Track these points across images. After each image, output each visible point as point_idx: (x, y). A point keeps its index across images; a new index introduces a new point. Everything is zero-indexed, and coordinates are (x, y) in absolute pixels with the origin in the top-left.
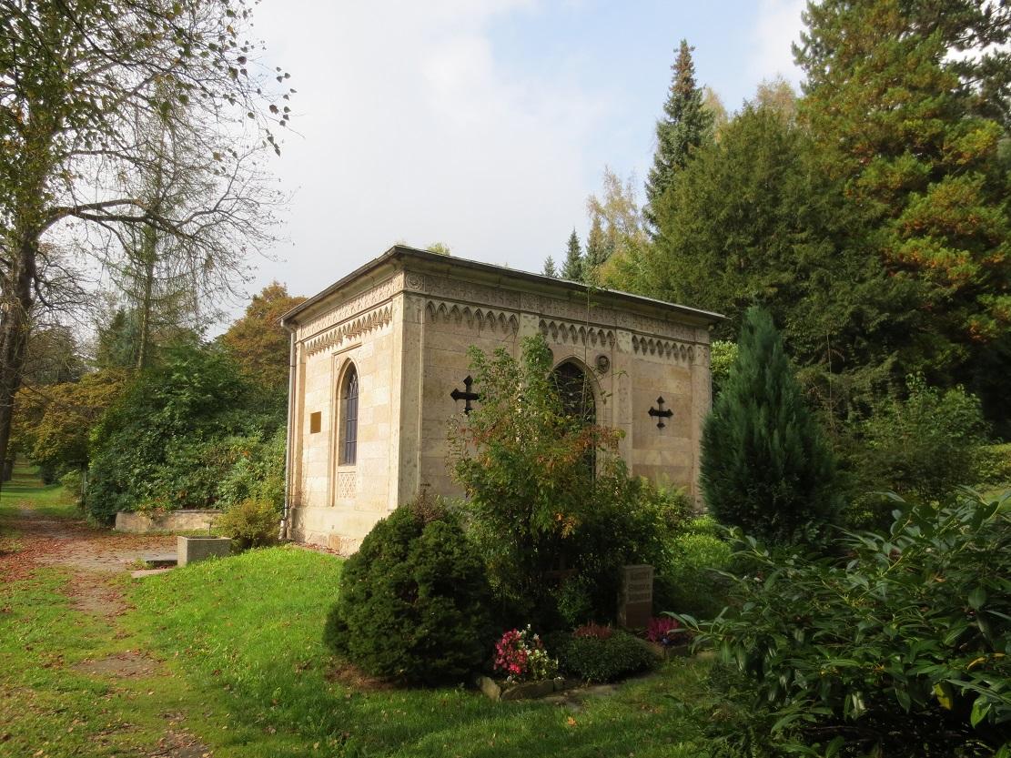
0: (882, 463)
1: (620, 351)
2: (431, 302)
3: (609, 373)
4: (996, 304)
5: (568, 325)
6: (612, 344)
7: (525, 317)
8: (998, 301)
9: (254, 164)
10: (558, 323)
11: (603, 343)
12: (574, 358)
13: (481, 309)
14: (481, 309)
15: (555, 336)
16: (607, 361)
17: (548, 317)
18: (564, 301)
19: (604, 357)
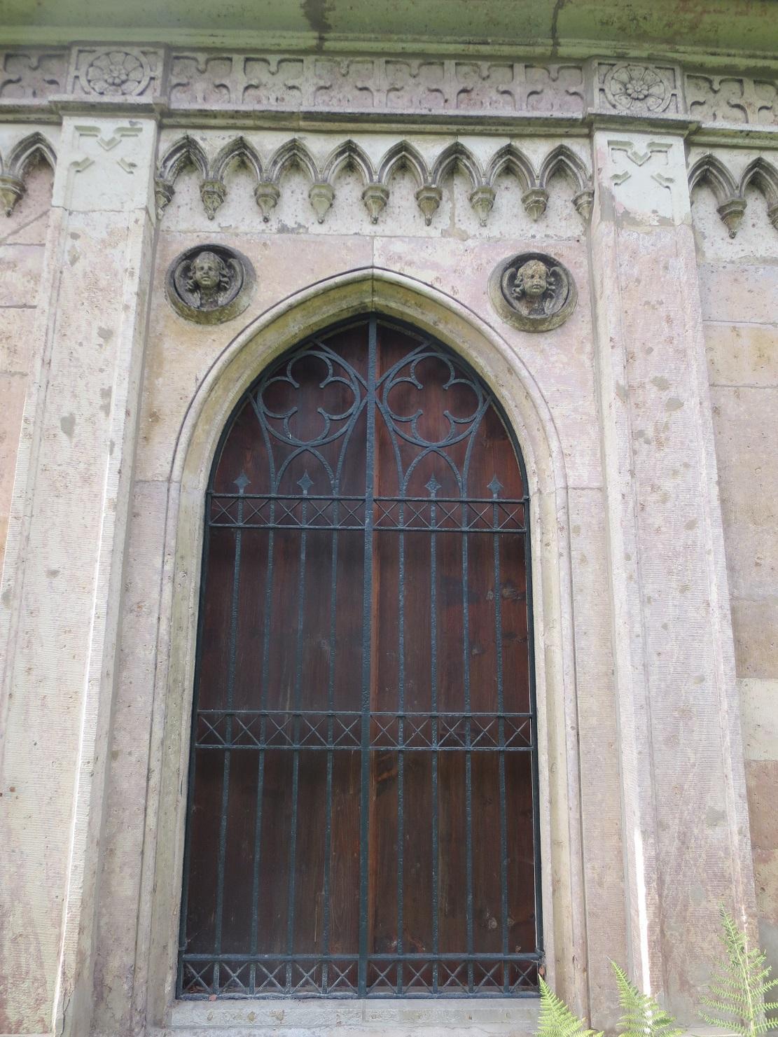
0: (114, 247)
1: (624, 219)
2: (561, 151)
3: (579, 327)
4: (553, 45)
5: (321, 147)
6: (583, 205)
7: (83, 131)
8: (550, 48)
9: (35, 744)
10: (268, 143)
11: (537, 206)
12: (374, 282)
13: (196, 135)
14: (196, 135)
15: (268, 198)
16: (224, 253)
17: (204, 120)
18: (295, 55)
19: (520, 261)
